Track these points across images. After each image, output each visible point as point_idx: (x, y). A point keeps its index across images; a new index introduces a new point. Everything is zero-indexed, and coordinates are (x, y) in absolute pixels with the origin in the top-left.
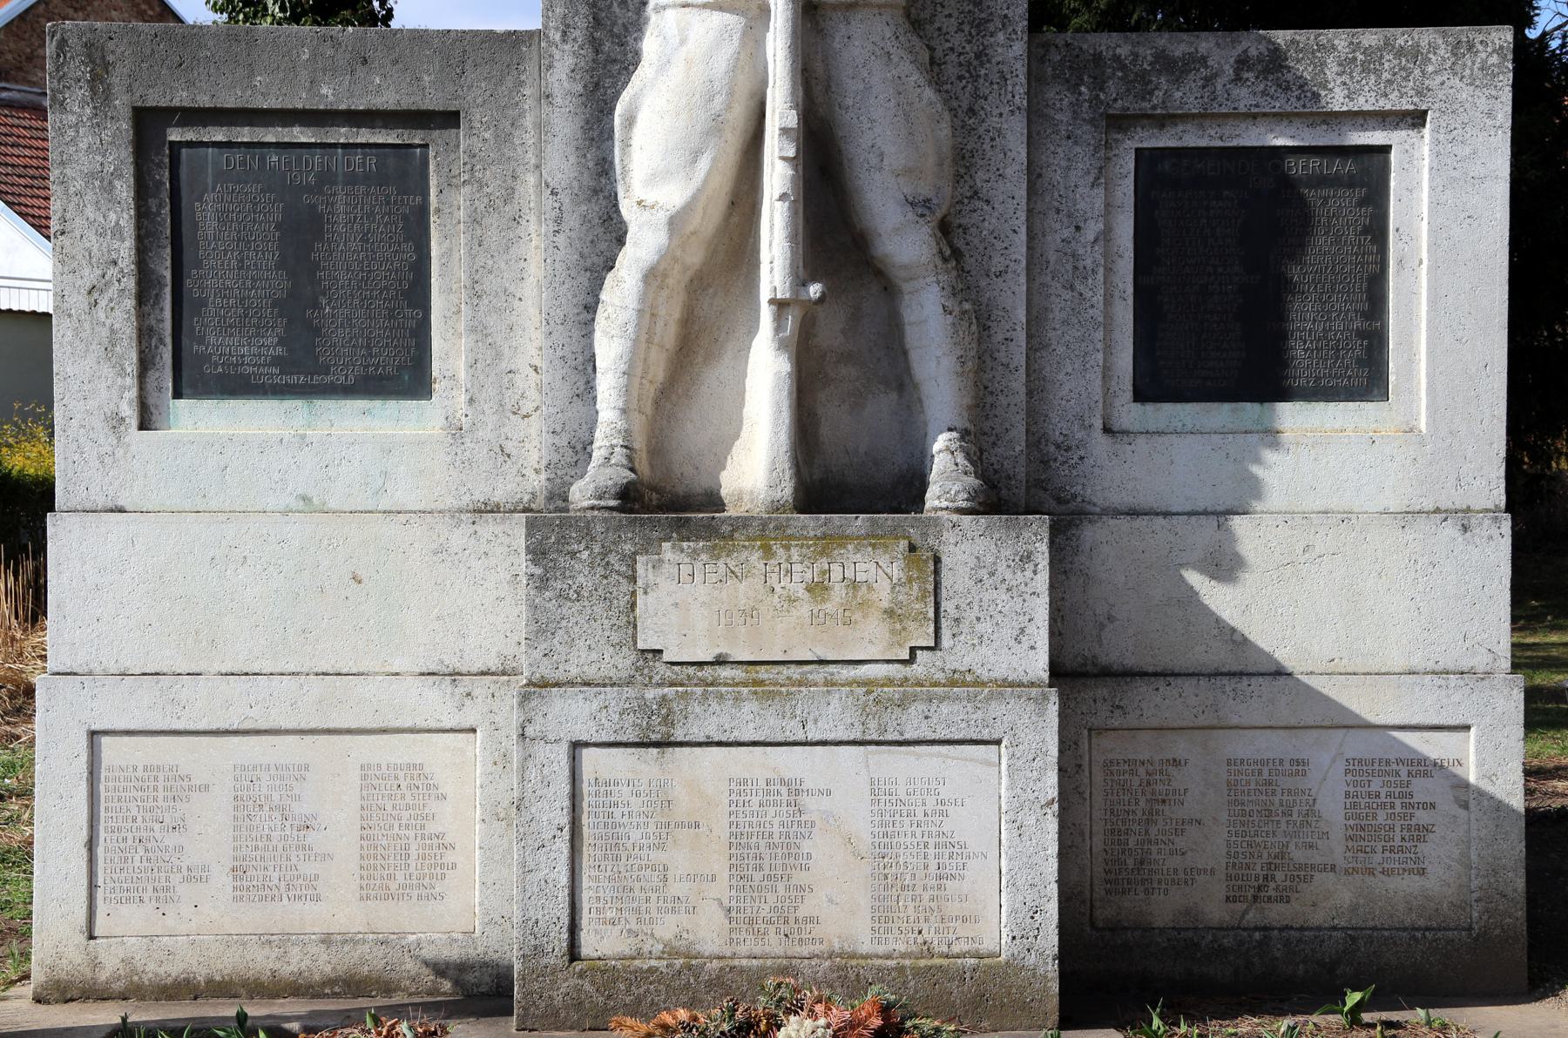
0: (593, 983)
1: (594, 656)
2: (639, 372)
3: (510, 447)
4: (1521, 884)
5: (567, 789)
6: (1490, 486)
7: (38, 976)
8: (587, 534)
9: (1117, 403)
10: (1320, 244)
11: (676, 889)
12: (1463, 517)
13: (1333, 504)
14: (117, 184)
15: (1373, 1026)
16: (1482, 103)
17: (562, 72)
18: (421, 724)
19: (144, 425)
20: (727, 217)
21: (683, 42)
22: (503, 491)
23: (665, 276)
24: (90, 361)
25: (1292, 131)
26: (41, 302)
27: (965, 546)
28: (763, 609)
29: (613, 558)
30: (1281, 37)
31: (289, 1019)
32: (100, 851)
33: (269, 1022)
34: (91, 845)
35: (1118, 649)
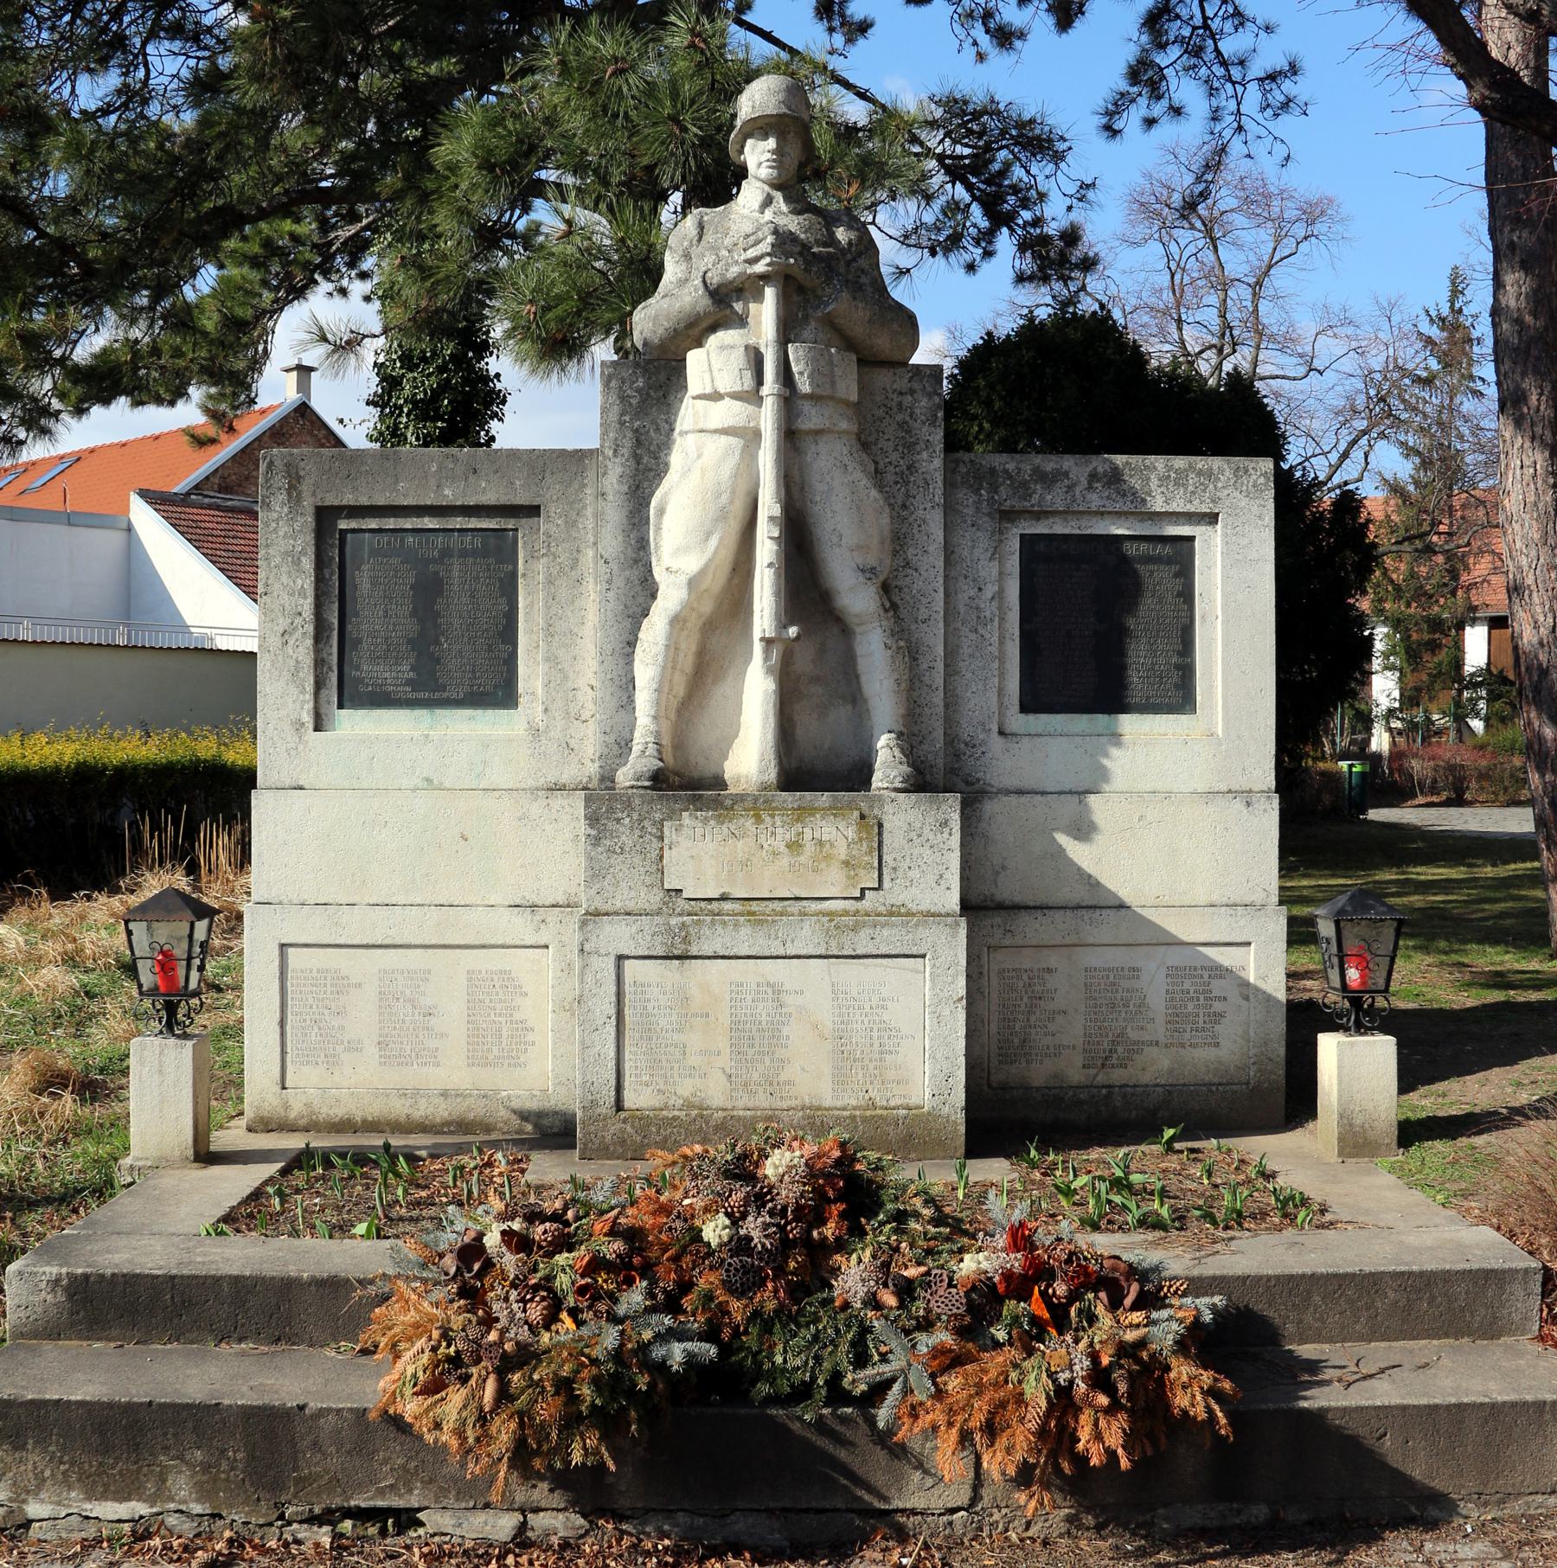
0: (633, 1126)
1: (633, 894)
2: (666, 690)
3: (572, 743)
4: (1282, 1051)
5: (613, 989)
6: (1265, 775)
7: (249, 1113)
8: (628, 805)
9: (1008, 713)
10: (1147, 604)
11: (693, 1060)
12: (1247, 796)
13: (1159, 786)
14: (303, 559)
15: (1181, 1152)
16: (1255, 509)
17: (613, 478)
18: (509, 941)
19: (316, 729)
20: (730, 580)
21: (699, 457)
22: (568, 775)
23: (685, 621)
24: (282, 682)
25: (1128, 524)
26: (250, 645)
27: (902, 816)
28: (755, 860)
29: (646, 823)
30: (1119, 459)
31: (419, 1148)
32: (288, 1028)
33: (406, 1150)
34: (282, 1023)
35: (1008, 890)
